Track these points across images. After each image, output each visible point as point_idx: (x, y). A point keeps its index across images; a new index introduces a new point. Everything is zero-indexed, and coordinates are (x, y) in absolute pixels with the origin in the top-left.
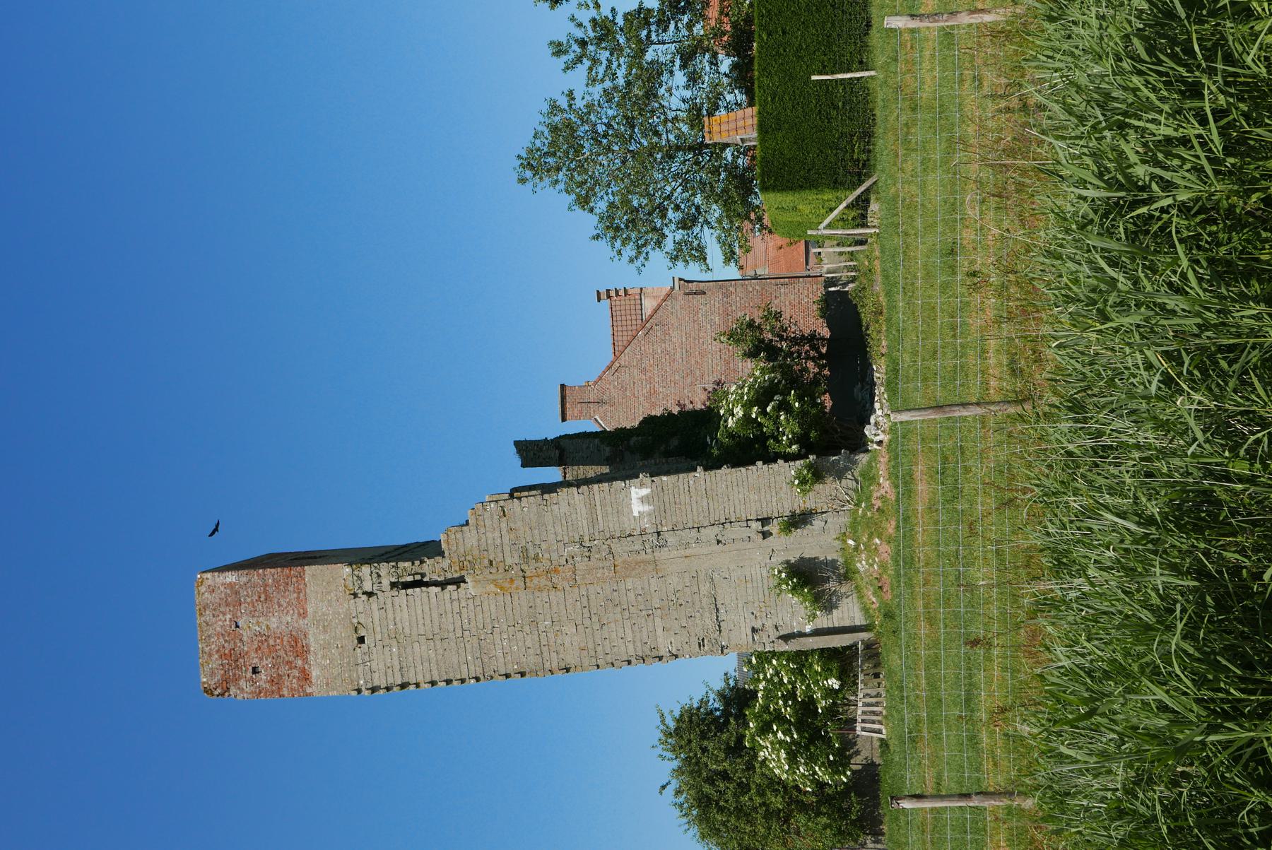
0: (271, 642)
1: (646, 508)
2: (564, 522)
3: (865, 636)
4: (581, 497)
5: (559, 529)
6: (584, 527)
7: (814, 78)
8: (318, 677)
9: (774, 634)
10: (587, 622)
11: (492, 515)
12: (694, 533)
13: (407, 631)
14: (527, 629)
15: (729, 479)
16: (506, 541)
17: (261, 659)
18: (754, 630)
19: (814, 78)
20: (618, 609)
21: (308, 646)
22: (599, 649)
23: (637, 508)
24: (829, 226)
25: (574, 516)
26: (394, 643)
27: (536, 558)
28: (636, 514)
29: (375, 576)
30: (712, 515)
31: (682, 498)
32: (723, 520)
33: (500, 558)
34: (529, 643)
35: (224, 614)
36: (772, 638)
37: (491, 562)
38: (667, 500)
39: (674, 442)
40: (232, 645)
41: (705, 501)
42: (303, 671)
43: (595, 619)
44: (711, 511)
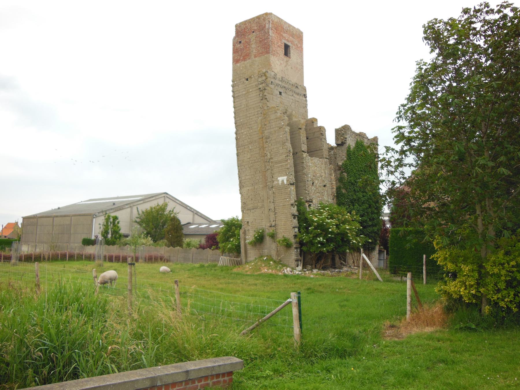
0: (248, 46)
1: (280, 182)
2: (277, 151)
3: (244, 260)
4: (284, 158)
5: (275, 149)
6: (275, 159)
7: (424, 256)
8: (237, 66)
9: (246, 229)
10: (251, 162)
11: (280, 124)
12: (272, 201)
13: (249, 96)
14: (249, 140)
15: (288, 214)
16: (272, 130)
17: (243, 44)
18: (248, 222)
19: (424, 256)
20: (254, 173)
21: (246, 60)
22: (243, 167)
23: (280, 179)
24: (364, 259)
25: (279, 155)
26: (246, 92)
27: (267, 142)
28: (279, 178)
29: (262, 82)
30: (277, 207)
31: (283, 196)
32: (276, 211)
33: (267, 128)
34: (245, 141)
35: (257, 26)
36: (245, 228)
37: (266, 125)
38: (283, 190)
39: (344, 191)
40: (248, 32)
41: (281, 205)
42: (239, 60)
43: (252, 165)
44: (279, 207)
